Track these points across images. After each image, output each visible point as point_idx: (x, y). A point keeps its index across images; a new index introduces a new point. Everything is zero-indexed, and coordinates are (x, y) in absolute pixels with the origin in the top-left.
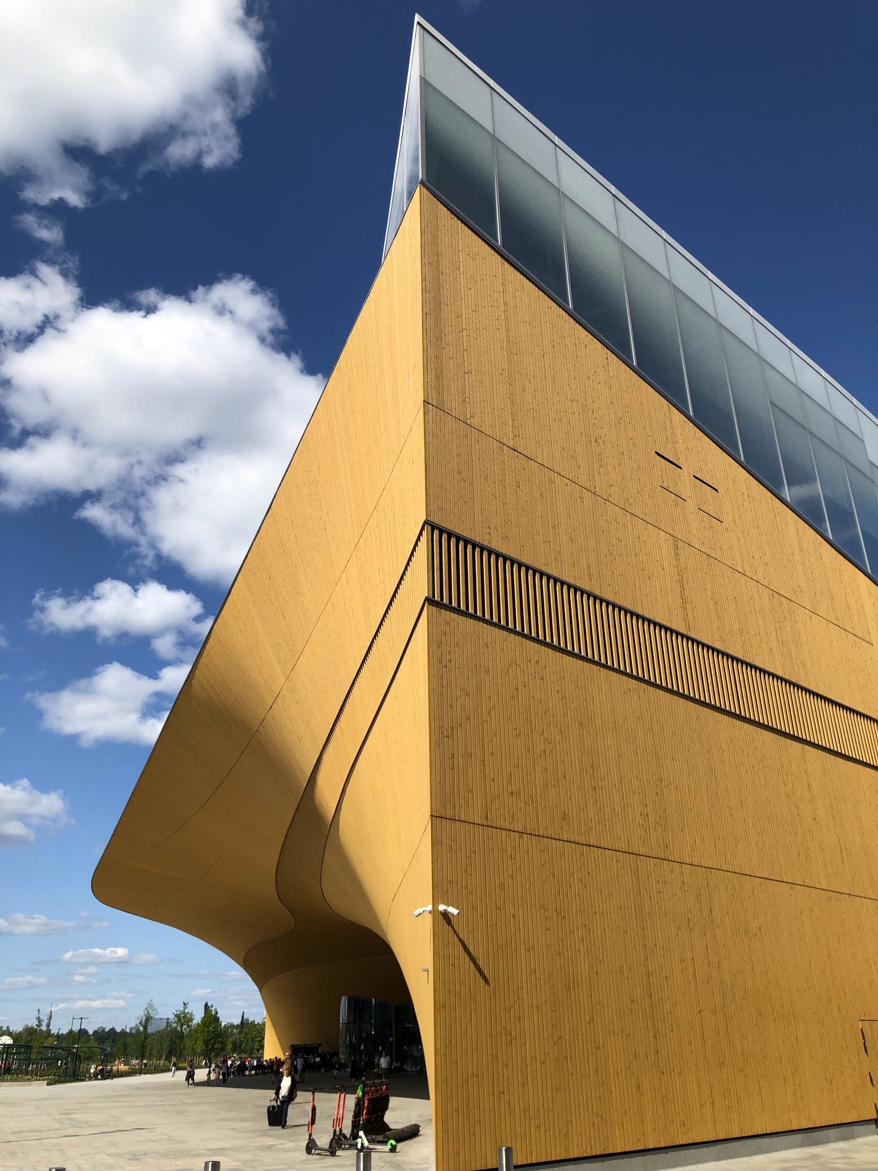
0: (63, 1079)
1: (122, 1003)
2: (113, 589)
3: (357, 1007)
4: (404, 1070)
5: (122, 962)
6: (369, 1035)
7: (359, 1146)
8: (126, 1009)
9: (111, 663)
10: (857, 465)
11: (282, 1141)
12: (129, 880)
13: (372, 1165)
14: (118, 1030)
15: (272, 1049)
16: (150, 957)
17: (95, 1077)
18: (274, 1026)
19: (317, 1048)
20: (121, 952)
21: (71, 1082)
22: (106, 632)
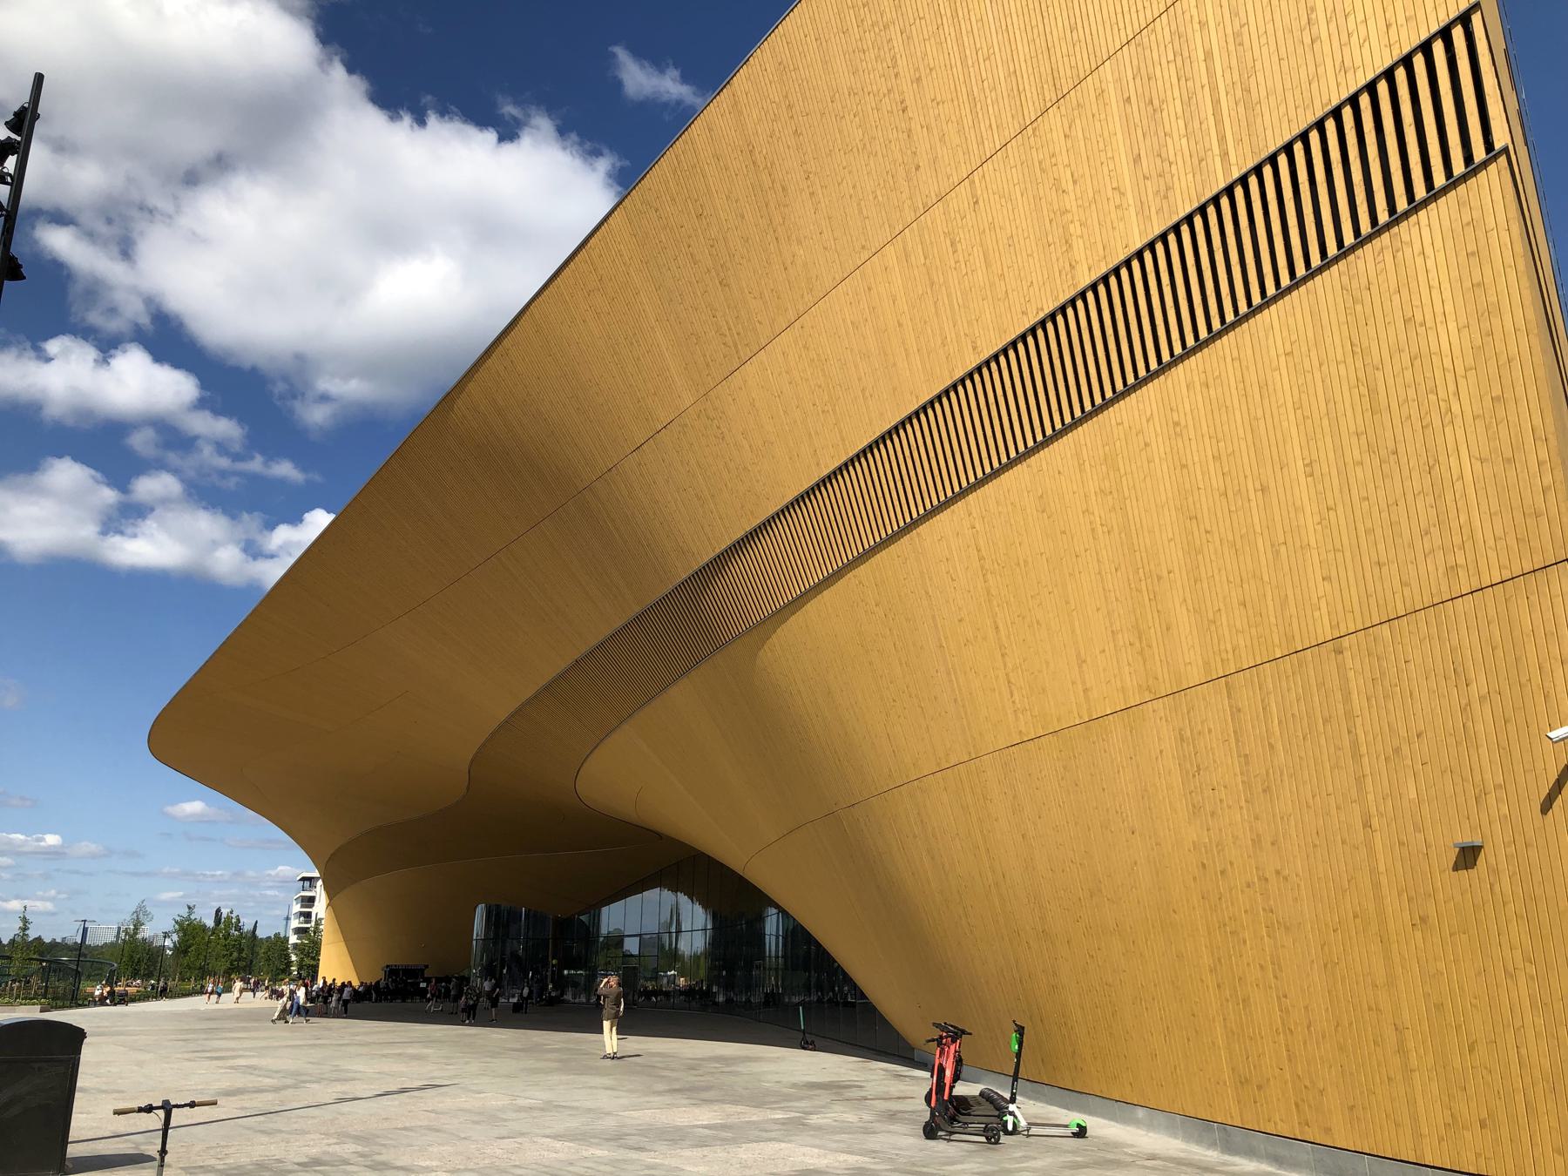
0: (60, 1003)
1: (49, 906)
2: (65, 353)
3: (499, 921)
4: (564, 1002)
5: (54, 854)
6: (514, 955)
7: (1010, 1127)
8: (53, 914)
9: (60, 457)
10: (1520, 247)
11: (739, 1108)
12: (205, 734)
13: (81, 1082)
14: (47, 940)
15: (335, 967)
16: (93, 847)
17: (102, 1001)
18: (346, 940)
19: (422, 971)
20: (52, 840)
21: (70, 1007)
22: (53, 411)
